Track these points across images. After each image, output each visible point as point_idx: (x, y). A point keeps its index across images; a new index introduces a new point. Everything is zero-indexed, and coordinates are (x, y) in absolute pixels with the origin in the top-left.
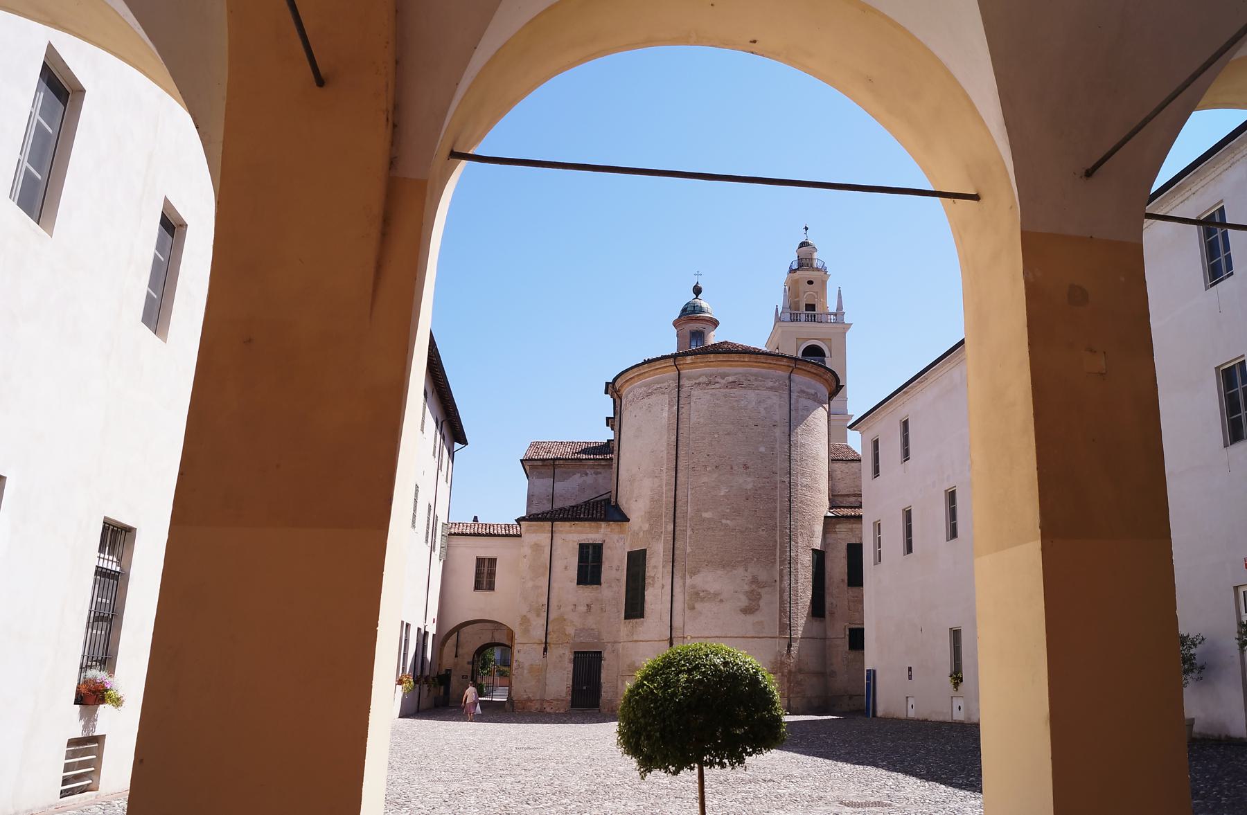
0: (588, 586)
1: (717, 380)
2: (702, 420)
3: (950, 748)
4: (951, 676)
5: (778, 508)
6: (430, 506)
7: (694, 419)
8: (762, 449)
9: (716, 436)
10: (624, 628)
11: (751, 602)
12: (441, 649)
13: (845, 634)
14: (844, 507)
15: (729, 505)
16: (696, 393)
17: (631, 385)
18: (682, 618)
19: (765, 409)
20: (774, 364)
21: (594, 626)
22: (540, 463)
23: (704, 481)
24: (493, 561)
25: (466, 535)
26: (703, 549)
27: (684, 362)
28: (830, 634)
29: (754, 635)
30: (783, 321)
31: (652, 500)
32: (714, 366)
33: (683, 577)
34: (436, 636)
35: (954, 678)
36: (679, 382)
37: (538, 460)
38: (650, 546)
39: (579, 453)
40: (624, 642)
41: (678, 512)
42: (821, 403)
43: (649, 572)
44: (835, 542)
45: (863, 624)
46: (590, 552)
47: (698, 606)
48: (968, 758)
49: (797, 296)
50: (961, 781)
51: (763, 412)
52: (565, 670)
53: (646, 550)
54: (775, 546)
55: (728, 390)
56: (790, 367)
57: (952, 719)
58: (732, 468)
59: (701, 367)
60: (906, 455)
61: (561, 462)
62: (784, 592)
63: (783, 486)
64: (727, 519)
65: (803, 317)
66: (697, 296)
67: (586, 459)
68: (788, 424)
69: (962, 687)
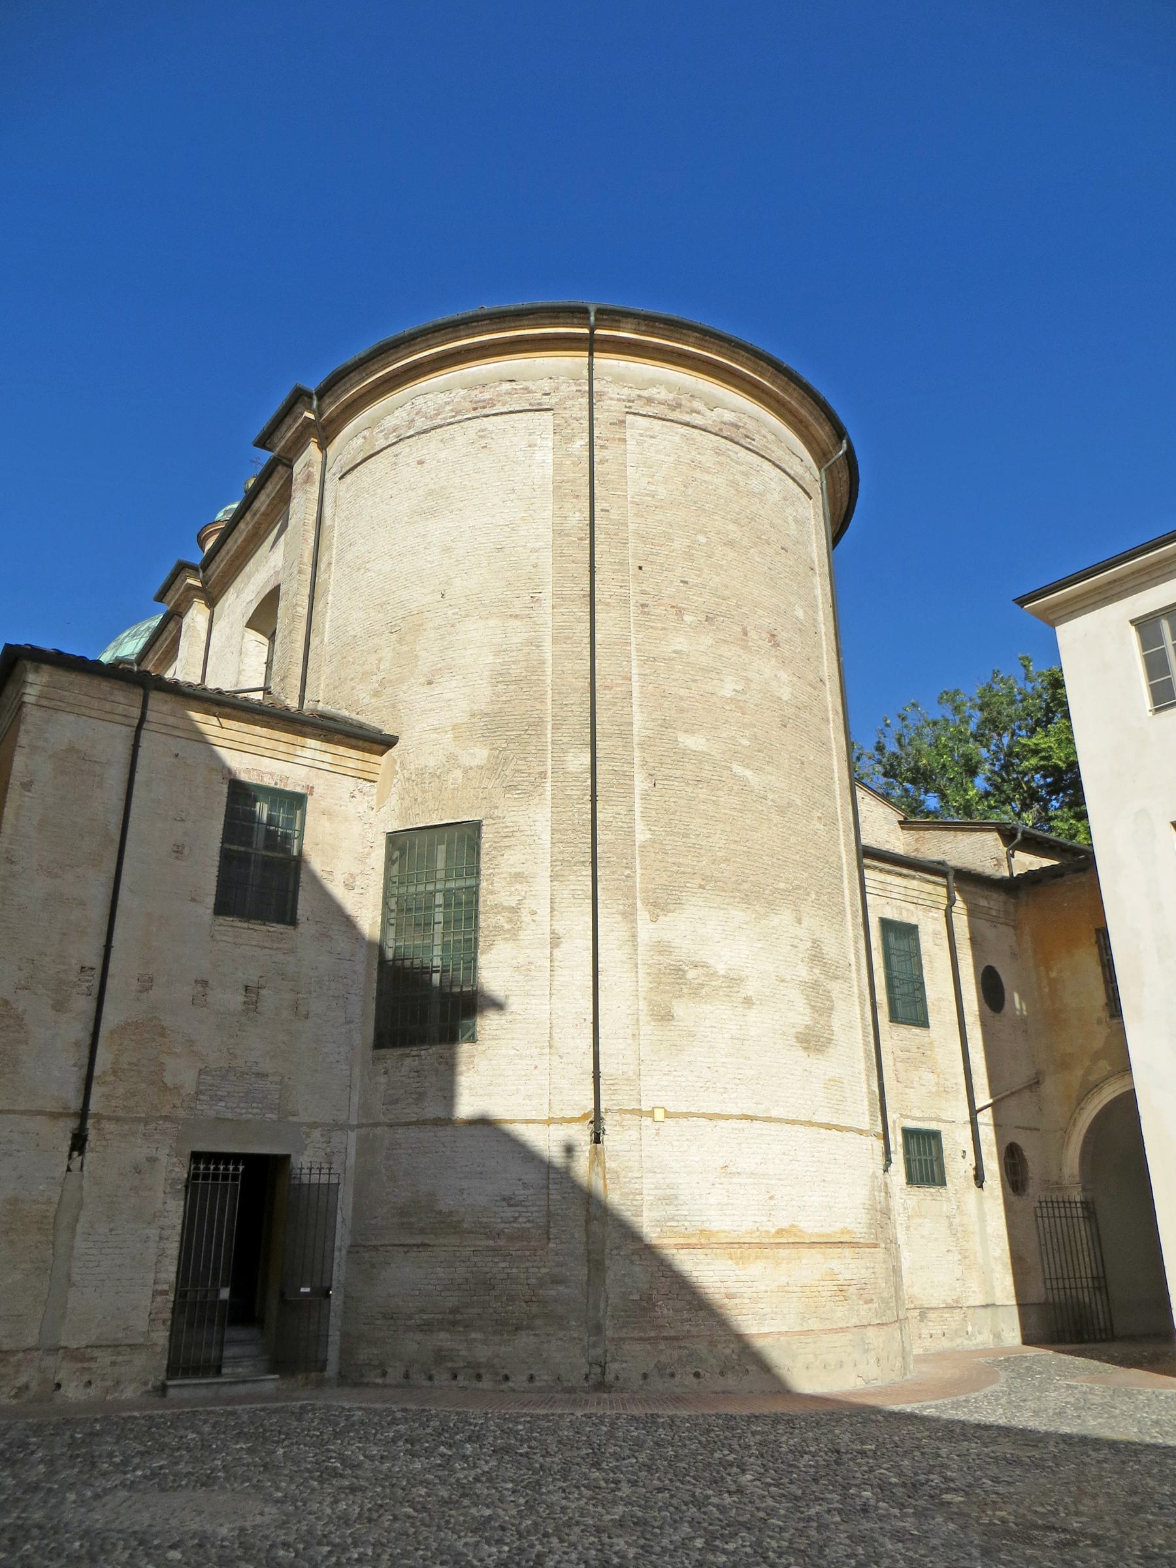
9: (702, 539)
23: (679, 648)
33: (629, 915)
47: (680, 1009)
64: (747, 766)
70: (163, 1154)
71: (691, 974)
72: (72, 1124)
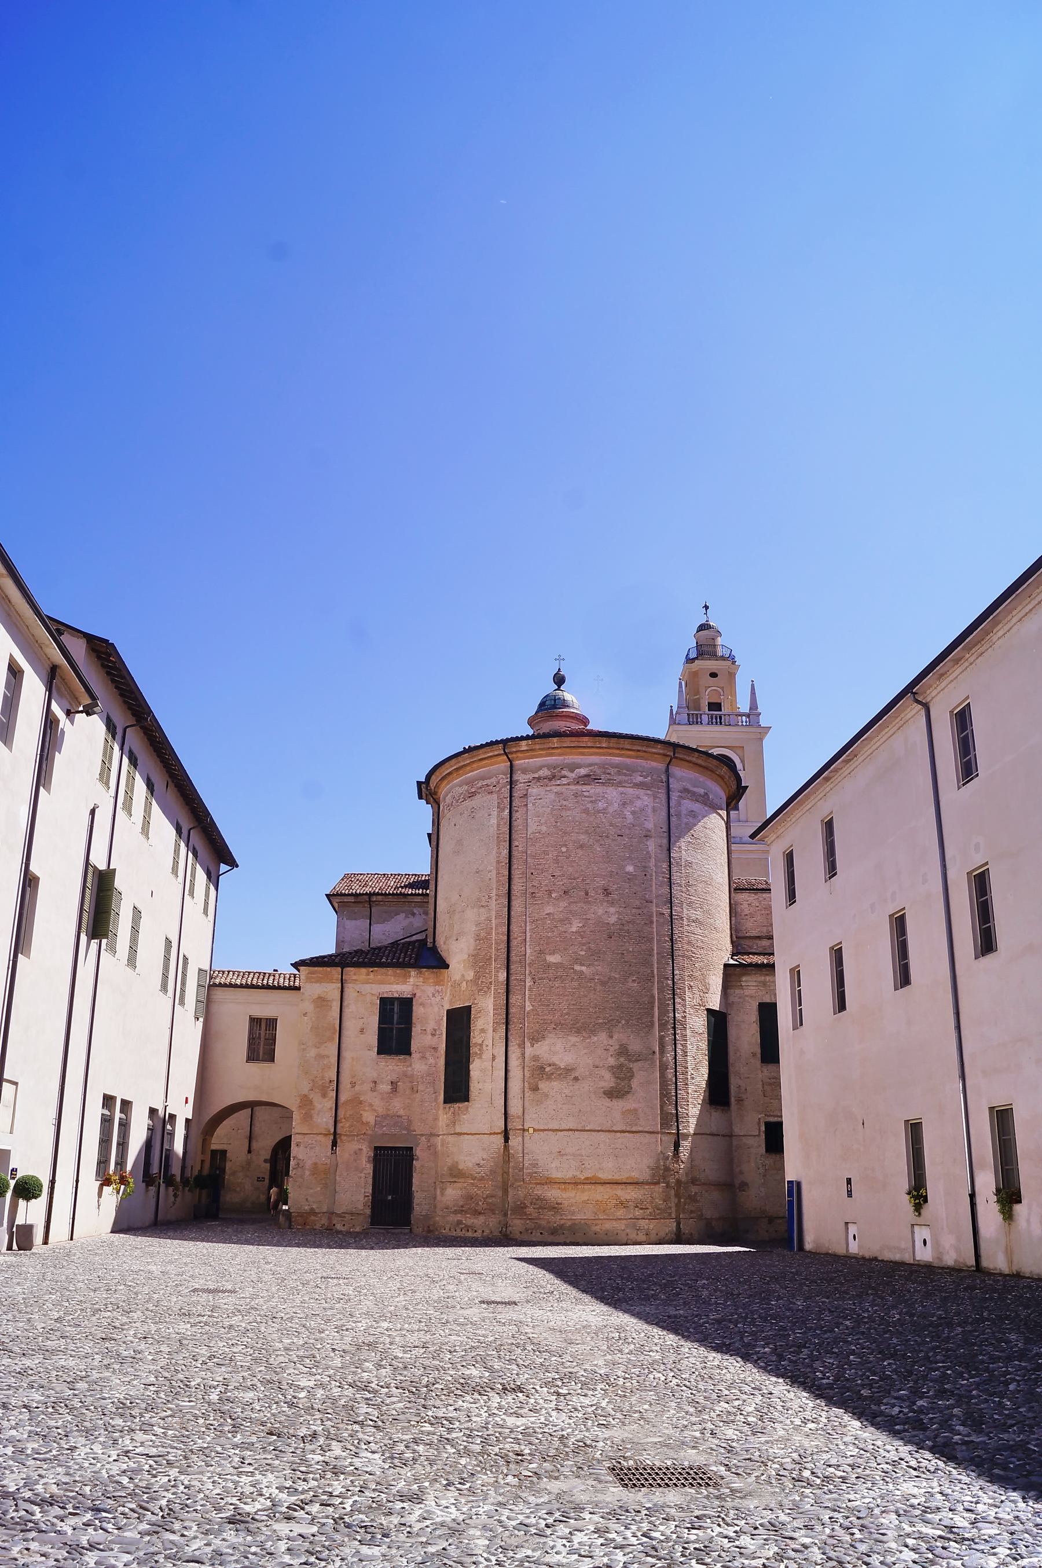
0: (392, 1057)
1: (564, 773)
2: (544, 829)
3: (897, 1316)
4: (909, 1194)
5: (655, 952)
6: (168, 942)
7: (532, 827)
8: (630, 868)
9: (564, 849)
10: (443, 1116)
11: (619, 1081)
12: (204, 1141)
13: (760, 1130)
14: (754, 954)
15: (584, 945)
16: (534, 791)
17: (448, 783)
18: (521, 1103)
19: (633, 813)
20: (645, 752)
21: (402, 1112)
22: (352, 899)
24: (272, 1023)
25: (236, 986)
26: (548, 1005)
27: (518, 749)
28: (737, 1130)
29: (624, 1128)
30: (679, 724)
31: (478, 938)
32: (560, 755)
33: (522, 1045)
34: (193, 1125)
35: (913, 1196)
36: (511, 777)
37: (349, 895)
38: (476, 1002)
39: (406, 886)
40: (444, 1135)
41: (513, 954)
42: (714, 808)
43: (476, 1038)
44: (741, 1000)
45: (781, 1116)
46: (395, 1010)
47: (542, 1085)
48: (924, 1343)
49: (697, 692)
50: (897, 1409)
51: (630, 818)
52: (361, 1172)
53: (470, 1007)
54: (652, 1003)
55: (579, 787)
56: (667, 756)
57: (914, 1259)
58: (587, 894)
59: (541, 756)
60: (832, 870)
61: (380, 898)
62: (667, 1069)
63: (662, 920)
64: (582, 965)
65: (705, 718)
66: (559, 687)
67: (412, 894)
68: (666, 834)
69: (927, 1210)
70: (364, 1147)
71: (548, 1069)
72: (332, 1137)
